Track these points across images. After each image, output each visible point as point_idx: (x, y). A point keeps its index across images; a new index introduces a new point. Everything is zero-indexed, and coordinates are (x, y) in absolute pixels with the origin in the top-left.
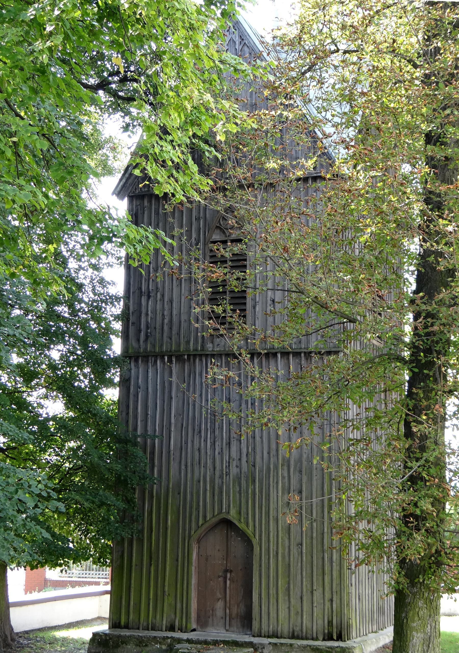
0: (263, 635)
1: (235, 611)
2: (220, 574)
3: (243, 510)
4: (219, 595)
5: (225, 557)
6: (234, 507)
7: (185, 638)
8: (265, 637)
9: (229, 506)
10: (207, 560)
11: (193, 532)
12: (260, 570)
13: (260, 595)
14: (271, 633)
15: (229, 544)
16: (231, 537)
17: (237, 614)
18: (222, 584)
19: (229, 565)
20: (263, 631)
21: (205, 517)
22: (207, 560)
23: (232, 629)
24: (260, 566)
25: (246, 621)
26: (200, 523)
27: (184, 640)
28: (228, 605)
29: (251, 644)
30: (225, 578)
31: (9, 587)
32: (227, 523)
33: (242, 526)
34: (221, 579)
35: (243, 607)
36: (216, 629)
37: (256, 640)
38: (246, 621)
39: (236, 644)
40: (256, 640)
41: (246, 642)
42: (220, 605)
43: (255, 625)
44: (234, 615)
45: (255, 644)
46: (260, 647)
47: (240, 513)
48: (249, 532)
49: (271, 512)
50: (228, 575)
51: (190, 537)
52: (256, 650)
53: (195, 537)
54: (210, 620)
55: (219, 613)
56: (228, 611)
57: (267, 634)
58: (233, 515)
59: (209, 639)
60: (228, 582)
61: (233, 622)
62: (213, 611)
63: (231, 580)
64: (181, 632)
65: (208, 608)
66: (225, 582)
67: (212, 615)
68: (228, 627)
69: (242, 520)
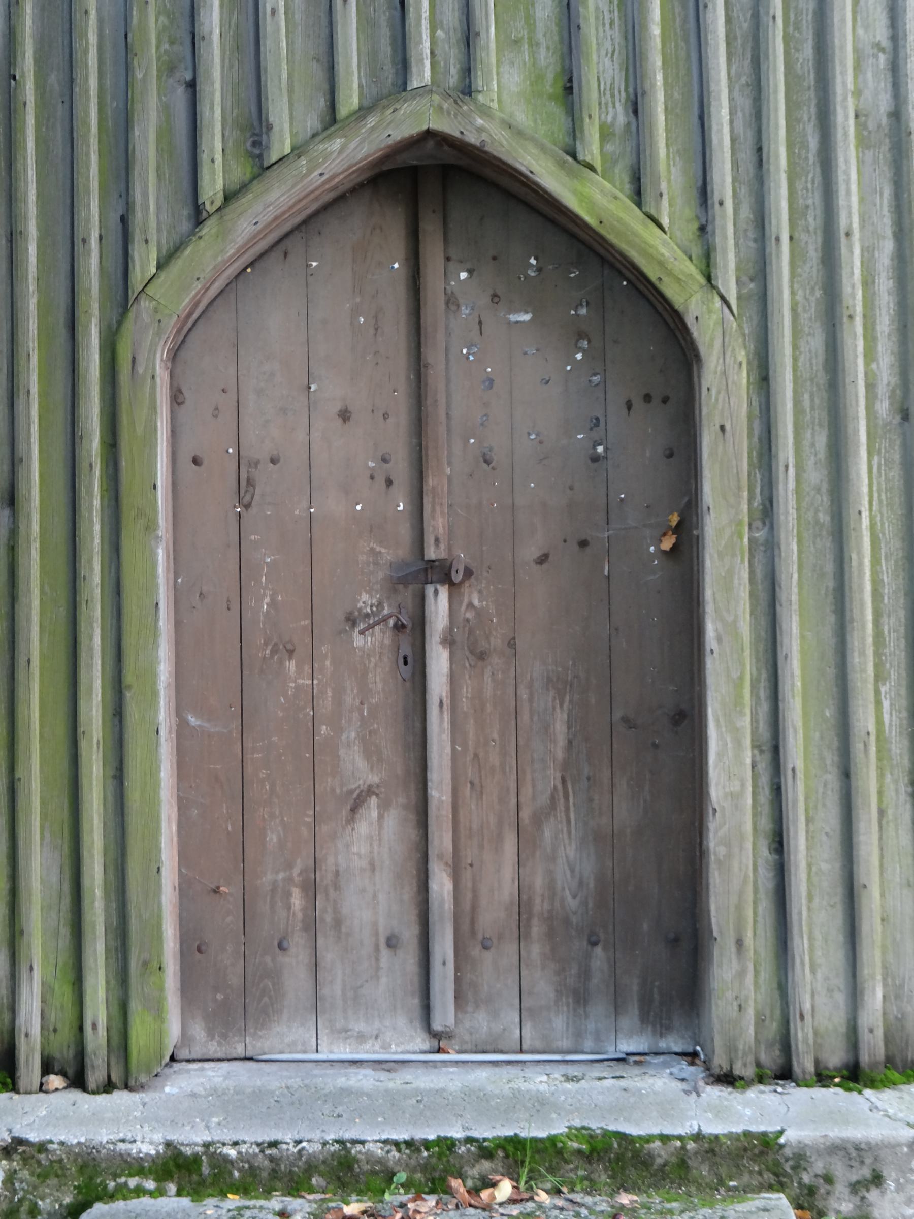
0: (805, 1063)
1: (500, 882)
2: (365, 601)
3: (600, 68)
4: (357, 768)
5: (401, 467)
6: (508, 43)
7: (148, 1145)
8: (822, 1078)
9: (469, 38)
10: (244, 490)
11: (144, 261)
12: (767, 553)
13: (774, 749)
14: (873, 1047)
15: (434, 356)
16: (451, 301)
17: (522, 908)
18: (382, 680)
19: (437, 523)
20: (803, 1035)
21: (254, 130)
22: (244, 490)
23: (481, 1022)
24: (767, 512)
25: (649, 954)
26: (213, 186)
27: (138, 1166)
28: (442, 839)
29: (761, 1160)
30: (413, 628)
31: (910, 15)
32: (438, 185)
33: (593, 198)
34: (372, 642)
35: (569, 850)
36: (344, 1033)
37: (797, 1116)
38: (649, 954)
39: (618, 1159)
40: (797, 1116)
41: (710, 1147)
42: (370, 842)
43: (736, 986)
44: (494, 913)
45: (800, 1159)
46: (843, 1175)
47: (569, 89)
48: (660, 247)
49: (844, 79)
50: (439, 605)
51: (123, 297)
52: (807, 1201)
53: (169, 297)
54: (294, 967)
55: (370, 899)
56: (441, 885)
57: (835, 1058)
58: (507, 116)
59: (373, 1135)
60: (439, 662)
61: (495, 970)
62: (311, 889)
63: (469, 647)
64: (78, 1081)
65: (268, 877)
66: (415, 666)
67: (312, 926)
68: (445, 1015)
69: (592, 149)
